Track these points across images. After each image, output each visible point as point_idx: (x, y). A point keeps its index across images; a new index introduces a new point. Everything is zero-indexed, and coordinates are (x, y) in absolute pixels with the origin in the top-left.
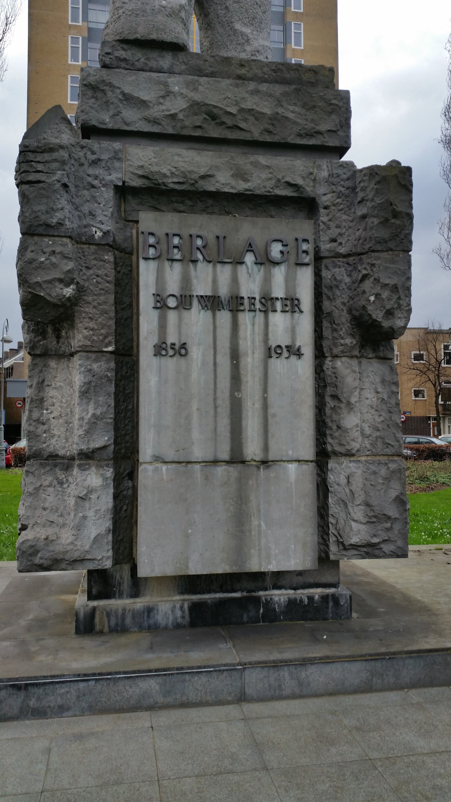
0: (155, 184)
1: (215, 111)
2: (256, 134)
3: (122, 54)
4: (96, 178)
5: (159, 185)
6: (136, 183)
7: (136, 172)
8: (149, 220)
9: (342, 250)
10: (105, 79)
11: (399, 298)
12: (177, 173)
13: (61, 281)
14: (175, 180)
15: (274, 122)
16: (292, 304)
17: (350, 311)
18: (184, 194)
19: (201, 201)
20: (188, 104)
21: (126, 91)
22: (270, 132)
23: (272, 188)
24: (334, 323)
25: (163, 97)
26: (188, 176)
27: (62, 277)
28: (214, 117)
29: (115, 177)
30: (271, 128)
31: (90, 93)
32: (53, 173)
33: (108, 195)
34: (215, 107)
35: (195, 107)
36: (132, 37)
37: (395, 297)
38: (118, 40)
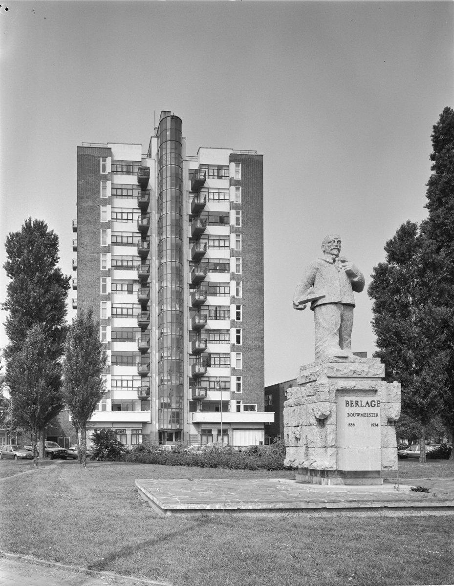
33: (335, 391)
35: (351, 371)
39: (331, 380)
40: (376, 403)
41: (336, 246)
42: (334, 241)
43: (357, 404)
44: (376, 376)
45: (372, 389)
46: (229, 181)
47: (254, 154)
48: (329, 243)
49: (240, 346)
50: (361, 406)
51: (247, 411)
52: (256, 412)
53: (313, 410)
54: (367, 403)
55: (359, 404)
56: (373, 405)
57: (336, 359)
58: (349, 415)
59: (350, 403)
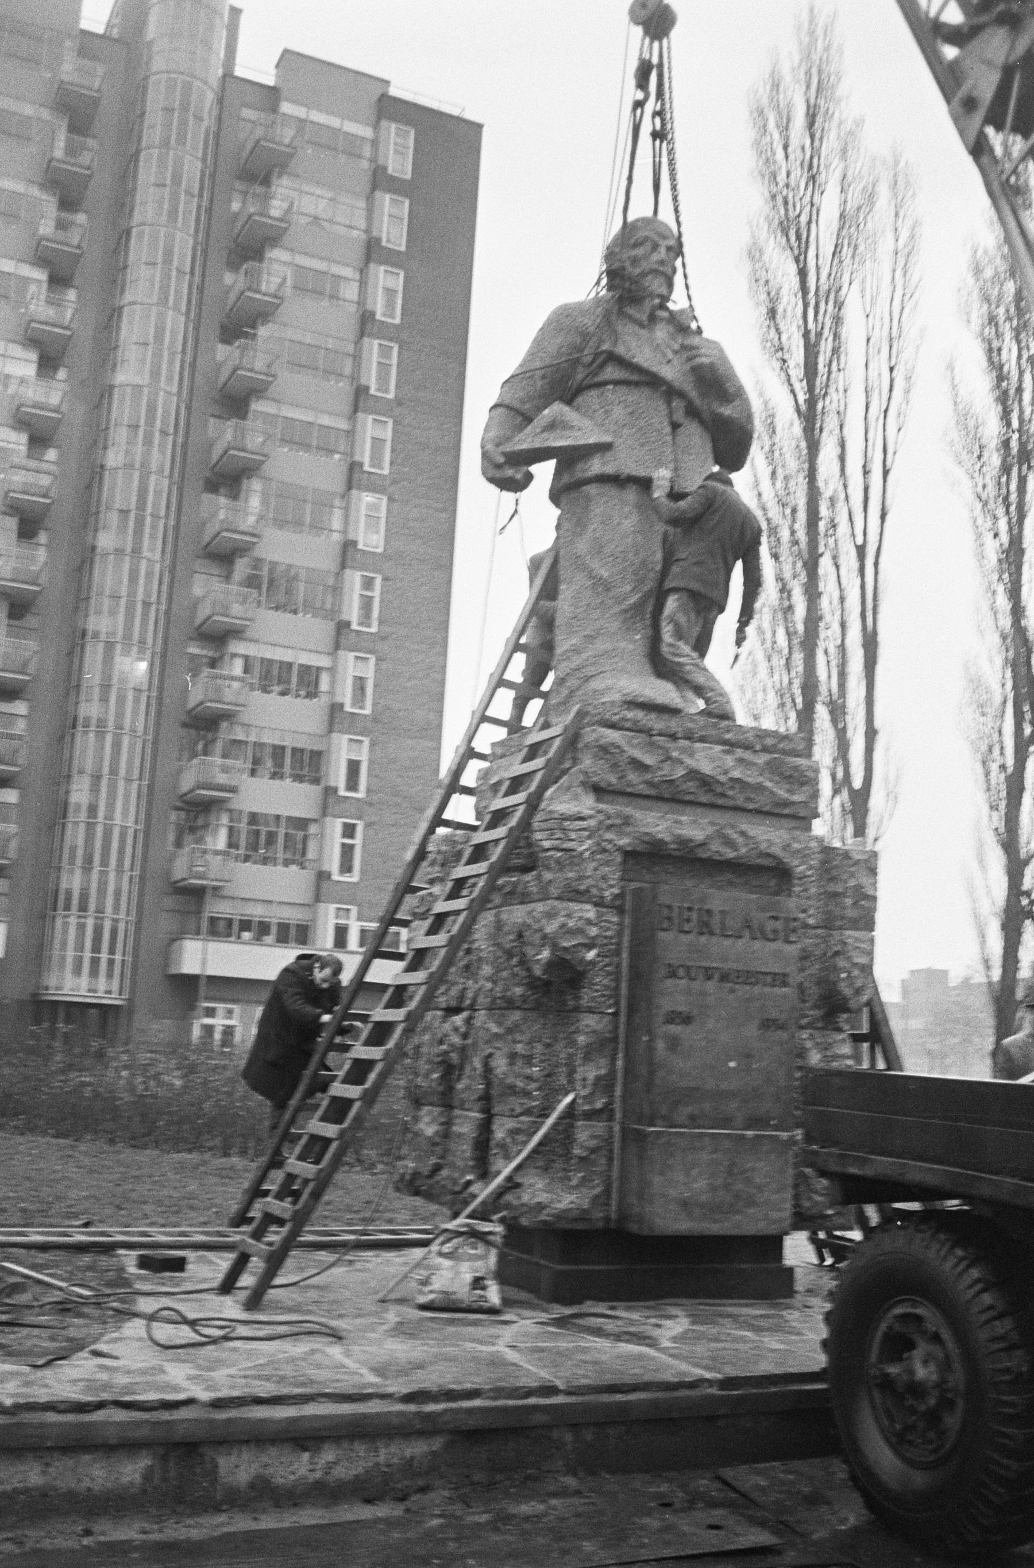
16: (146, 1089)
25: (662, 761)
35: (693, 774)
41: (662, 262)
42: (655, 247)
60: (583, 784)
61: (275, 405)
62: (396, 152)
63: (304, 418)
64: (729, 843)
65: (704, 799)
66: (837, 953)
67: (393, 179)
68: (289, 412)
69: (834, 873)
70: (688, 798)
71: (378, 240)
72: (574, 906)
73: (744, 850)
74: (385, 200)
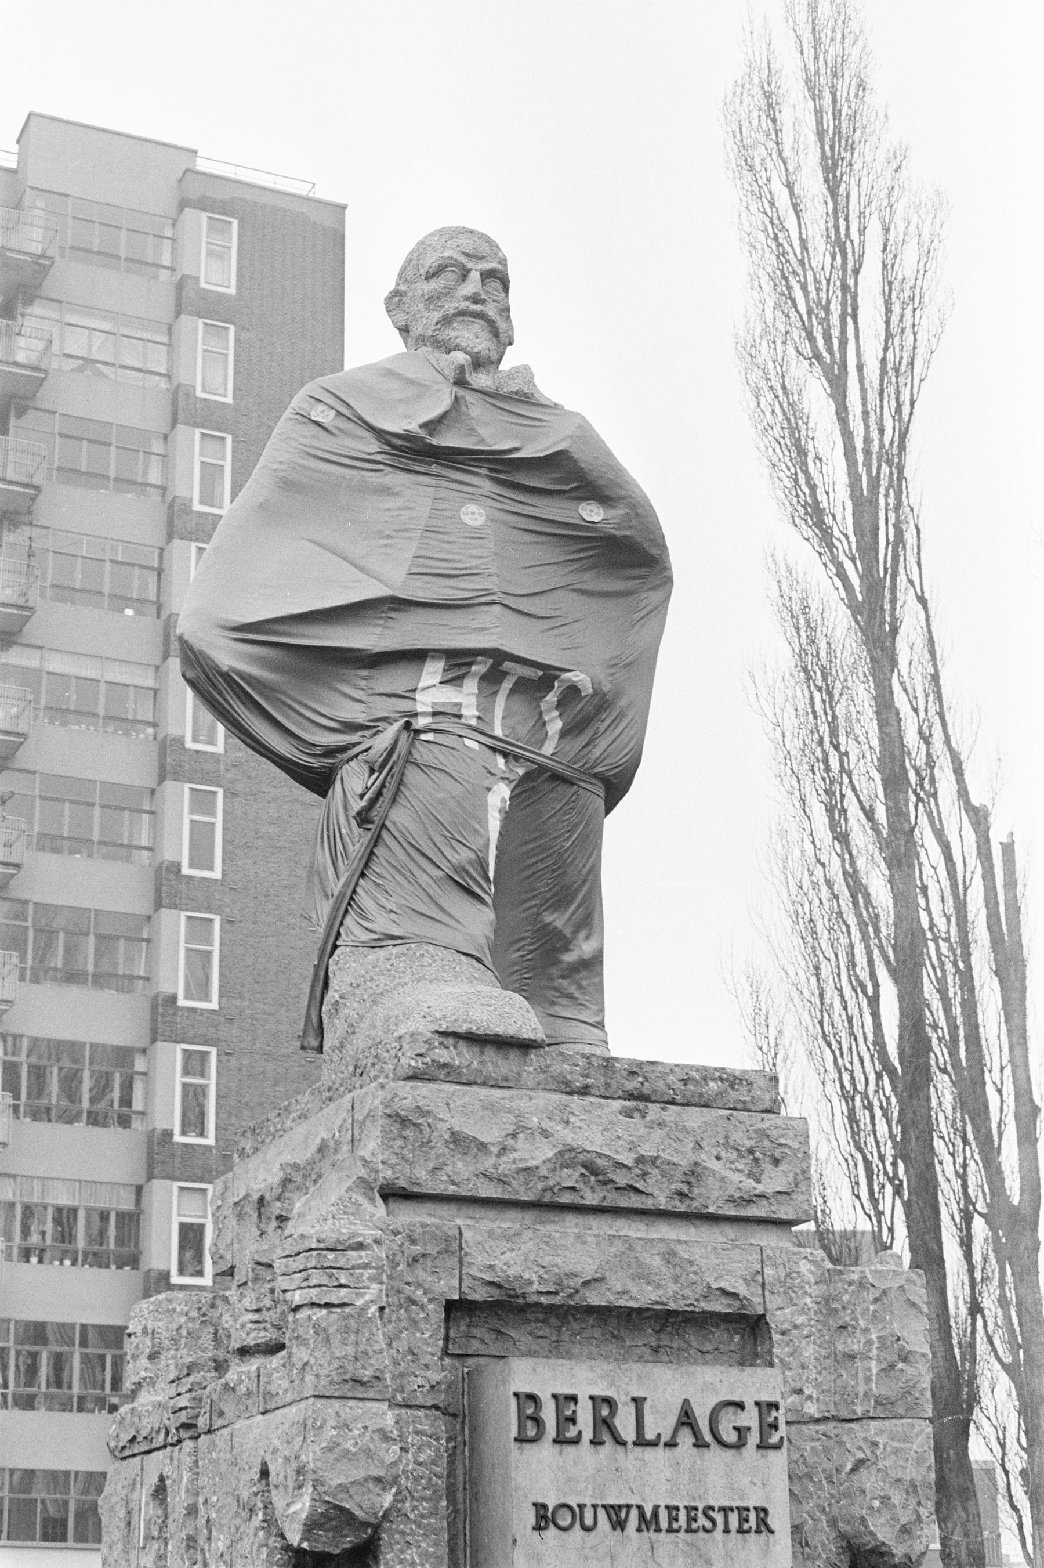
0: (510, 1296)
1: (600, 1162)
2: (662, 1201)
3: (443, 1055)
4: (419, 1285)
5: (517, 1297)
6: (480, 1295)
7: (479, 1275)
8: (533, 1373)
9: (811, 1409)
10: (420, 1104)
11: (919, 1504)
12: (546, 1276)
13: (378, 1480)
14: (543, 1289)
15: (691, 1179)
17: (833, 1523)
18: (551, 1310)
19: (575, 1320)
20: (555, 1151)
21: (457, 1128)
22: (681, 1194)
23: (697, 1300)
24: (807, 1544)
26: (565, 1282)
27: (382, 1473)
28: (592, 1169)
29: (448, 1287)
30: (685, 1188)
31: (395, 1128)
32: (358, 1288)
33: (436, 1313)
34: (600, 1155)
35: (567, 1157)
36: (463, 1028)
37: (913, 1502)
38: (437, 1032)
39: (409, 1216)
40: (750, 1418)
41: (476, 299)
42: (464, 275)
43: (604, 1426)
44: (752, 1211)
45: (719, 1306)
46: (740, 1057)
47: (304, 193)
48: (429, 277)
49: (207, 1148)
50: (641, 1442)
51: (86, 1541)
52: (70, 1544)
53: (265, 1473)
54: (686, 1419)
55: (625, 1424)
56: (731, 1437)
57: (462, 1057)
58: (544, 1518)
59: (549, 1414)
60: (364, 1184)
61: (37, 653)
62: (210, 254)
63: (83, 673)
64: (645, 1277)
65: (591, 1198)
66: (859, 1465)
67: (205, 295)
68: (57, 664)
69: (846, 1318)
70: (566, 1198)
71: (190, 393)
72: (350, 1409)
73: (672, 1287)
74: (194, 329)
